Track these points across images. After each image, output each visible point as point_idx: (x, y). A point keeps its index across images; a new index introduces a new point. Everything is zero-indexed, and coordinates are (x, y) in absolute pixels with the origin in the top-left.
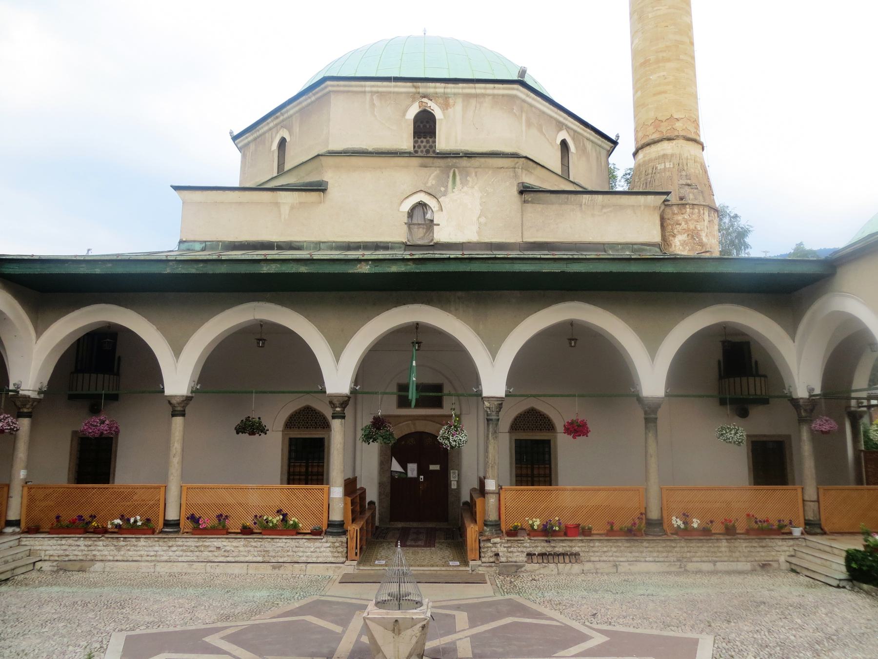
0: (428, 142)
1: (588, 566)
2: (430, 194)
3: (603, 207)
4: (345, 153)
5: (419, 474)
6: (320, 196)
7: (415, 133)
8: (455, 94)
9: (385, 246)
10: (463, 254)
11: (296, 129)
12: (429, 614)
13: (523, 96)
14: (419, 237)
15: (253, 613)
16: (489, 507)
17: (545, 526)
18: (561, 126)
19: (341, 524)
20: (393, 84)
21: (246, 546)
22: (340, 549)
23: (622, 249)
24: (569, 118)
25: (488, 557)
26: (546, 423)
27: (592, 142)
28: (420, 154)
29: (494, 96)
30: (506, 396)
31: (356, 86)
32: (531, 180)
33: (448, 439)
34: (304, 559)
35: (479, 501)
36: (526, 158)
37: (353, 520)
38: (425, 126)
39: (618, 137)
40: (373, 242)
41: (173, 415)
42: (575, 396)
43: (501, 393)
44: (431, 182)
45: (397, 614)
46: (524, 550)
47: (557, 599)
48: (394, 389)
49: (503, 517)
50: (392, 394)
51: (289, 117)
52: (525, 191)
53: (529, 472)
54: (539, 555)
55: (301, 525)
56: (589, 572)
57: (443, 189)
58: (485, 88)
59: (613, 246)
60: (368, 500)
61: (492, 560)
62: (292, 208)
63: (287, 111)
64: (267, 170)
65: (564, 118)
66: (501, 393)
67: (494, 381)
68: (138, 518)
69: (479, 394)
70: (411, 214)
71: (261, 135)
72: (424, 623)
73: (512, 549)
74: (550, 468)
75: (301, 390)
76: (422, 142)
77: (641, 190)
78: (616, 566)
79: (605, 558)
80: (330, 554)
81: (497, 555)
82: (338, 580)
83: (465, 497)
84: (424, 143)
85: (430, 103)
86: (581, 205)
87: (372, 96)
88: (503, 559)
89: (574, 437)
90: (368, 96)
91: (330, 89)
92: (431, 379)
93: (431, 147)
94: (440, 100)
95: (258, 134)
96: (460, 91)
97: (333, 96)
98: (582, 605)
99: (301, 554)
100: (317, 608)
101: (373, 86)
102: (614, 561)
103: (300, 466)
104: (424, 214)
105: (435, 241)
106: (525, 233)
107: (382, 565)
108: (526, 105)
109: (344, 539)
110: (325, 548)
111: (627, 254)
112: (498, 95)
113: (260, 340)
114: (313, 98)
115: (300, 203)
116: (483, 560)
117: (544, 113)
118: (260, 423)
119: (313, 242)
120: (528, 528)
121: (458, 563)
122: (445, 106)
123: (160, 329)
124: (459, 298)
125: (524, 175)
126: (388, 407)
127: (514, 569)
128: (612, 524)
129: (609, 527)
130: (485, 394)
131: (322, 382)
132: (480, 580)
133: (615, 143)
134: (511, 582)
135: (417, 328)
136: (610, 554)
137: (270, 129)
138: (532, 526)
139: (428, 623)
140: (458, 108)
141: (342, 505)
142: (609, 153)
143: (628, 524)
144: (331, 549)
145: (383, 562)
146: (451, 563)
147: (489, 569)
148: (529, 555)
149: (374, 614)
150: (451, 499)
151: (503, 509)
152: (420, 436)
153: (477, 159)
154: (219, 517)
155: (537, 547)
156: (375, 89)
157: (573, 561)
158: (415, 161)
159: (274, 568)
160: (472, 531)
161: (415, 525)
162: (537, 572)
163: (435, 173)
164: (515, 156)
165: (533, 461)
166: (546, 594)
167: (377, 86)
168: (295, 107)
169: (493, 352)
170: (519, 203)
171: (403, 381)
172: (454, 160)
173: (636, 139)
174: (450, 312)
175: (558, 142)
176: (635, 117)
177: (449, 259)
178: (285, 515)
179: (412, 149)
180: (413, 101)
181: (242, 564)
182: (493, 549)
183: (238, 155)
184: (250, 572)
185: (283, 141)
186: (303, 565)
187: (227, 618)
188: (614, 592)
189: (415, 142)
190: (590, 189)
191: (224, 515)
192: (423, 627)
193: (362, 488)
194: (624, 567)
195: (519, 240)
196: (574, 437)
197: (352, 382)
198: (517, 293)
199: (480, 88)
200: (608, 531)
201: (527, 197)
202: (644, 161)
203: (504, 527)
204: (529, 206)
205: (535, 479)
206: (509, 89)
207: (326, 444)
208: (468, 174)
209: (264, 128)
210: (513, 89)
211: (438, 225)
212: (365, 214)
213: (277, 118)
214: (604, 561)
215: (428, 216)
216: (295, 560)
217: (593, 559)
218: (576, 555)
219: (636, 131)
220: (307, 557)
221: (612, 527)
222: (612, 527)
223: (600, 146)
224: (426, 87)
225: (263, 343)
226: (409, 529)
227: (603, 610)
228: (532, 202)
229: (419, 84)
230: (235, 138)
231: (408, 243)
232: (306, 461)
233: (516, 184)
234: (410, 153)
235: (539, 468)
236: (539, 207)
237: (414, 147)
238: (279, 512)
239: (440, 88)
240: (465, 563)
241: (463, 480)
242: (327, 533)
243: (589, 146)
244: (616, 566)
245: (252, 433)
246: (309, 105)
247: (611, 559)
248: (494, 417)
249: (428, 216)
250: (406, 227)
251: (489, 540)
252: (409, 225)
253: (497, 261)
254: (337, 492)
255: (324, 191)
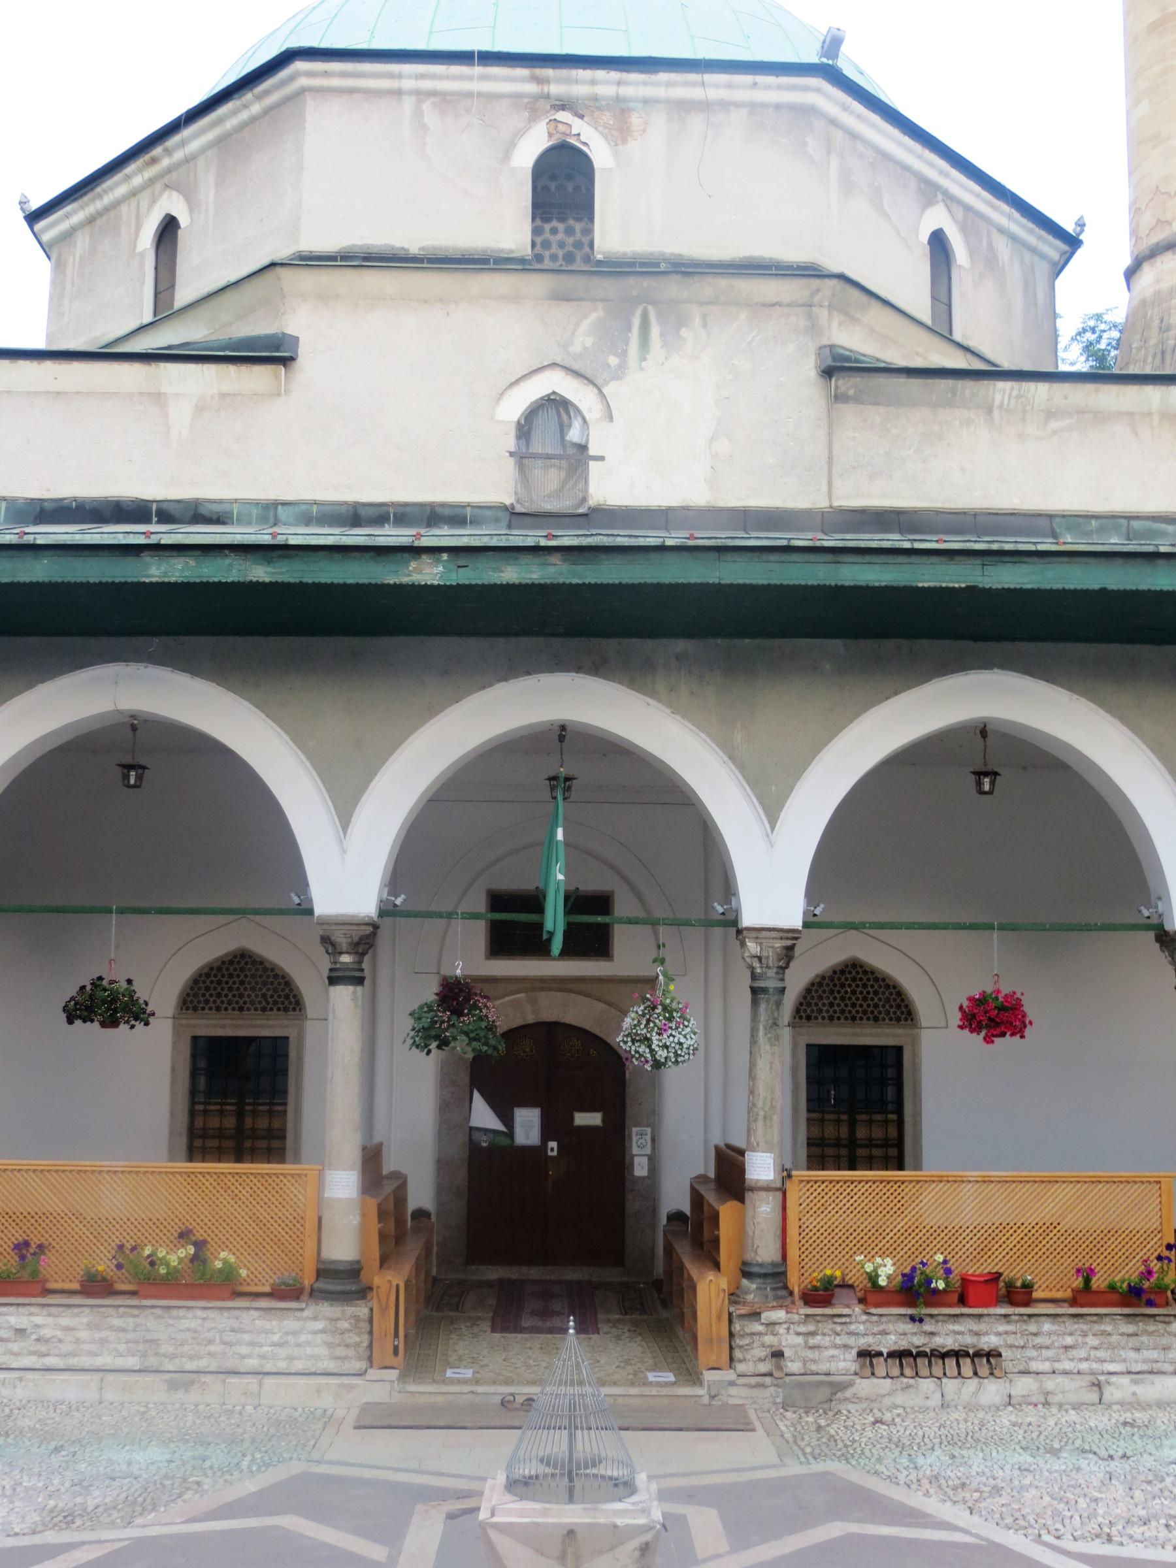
0: (570, 231)
1: (1023, 1386)
2: (577, 374)
3: (1050, 414)
4: (344, 258)
5: (546, 1136)
6: (277, 377)
7: (535, 205)
8: (646, 102)
9: (455, 516)
10: (692, 537)
11: (207, 191)
12: (657, 1515)
13: (832, 110)
14: (548, 492)
15: (135, 1506)
16: (756, 1227)
17: (908, 1278)
18: (930, 192)
19: (353, 1272)
20: (478, 70)
21: (98, 1327)
22: (353, 1338)
23: (1101, 530)
24: (954, 173)
25: (753, 1360)
26: (894, 1005)
27: (1013, 238)
28: (548, 263)
29: (753, 107)
30: (806, 925)
31: (375, 76)
32: (855, 339)
33: (647, 1040)
34: (252, 1363)
35: (727, 1211)
36: (842, 277)
37: (384, 1261)
38: (562, 187)
39: (1081, 225)
40: (422, 505)
41: (333, 981)
42: (990, 927)
43: (791, 916)
44: (583, 339)
45: (572, 1515)
46: (851, 1341)
47: (954, 1474)
48: (481, 906)
49: (793, 1253)
50: (476, 916)
51: (187, 160)
52: (838, 368)
53: (844, 1132)
54: (891, 1355)
55: (243, 1272)
56: (1026, 1401)
57: (613, 361)
58: (729, 86)
59: (1076, 520)
60: (412, 1205)
61: (763, 1368)
62: (200, 409)
63: (183, 144)
64: (123, 307)
65: (941, 172)
66: (791, 916)
67: (772, 883)
68: (223, 1255)
69: (731, 922)
70: (525, 428)
71: (107, 210)
72: (648, 1537)
73: (817, 1340)
74: (900, 1123)
75: (224, 905)
76: (554, 231)
77: (1148, 370)
78: (1098, 1385)
79: (1067, 1365)
80: (323, 1351)
81: (778, 1355)
82: (351, 1420)
83: (675, 1196)
84: (559, 232)
85: (578, 125)
86: (990, 410)
87: (419, 102)
88: (794, 1367)
89: (988, 1040)
90: (409, 103)
91: (303, 81)
92: (592, 884)
93: (578, 245)
94: (607, 118)
95: (99, 205)
96: (661, 92)
97: (310, 102)
98: (1023, 1488)
99: (244, 1350)
100: (312, 1494)
101: (422, 76)
102: (1092, 1373)
103: (221, 1113)
104: (563, 429)
105: (591, 502)
106: (838, 483)
107: (465, 1382)
108: (839, 135)
109: (361, 1310)
110: (310, 1336)
111: (1115, 542)
112: (765, 105)
113: (129, 767)
114: (256, 108)
115: (223, 395)
116: (741, 1367)
117: (885, 156)
118: (131, 994)
119: (256, 503)
120: (862, 1283)
121: (670, 1377)
122: (621, 133)
123: (299, 739)
124: (679, 657)
125: (835, 324)
126: (467, 956)
127: (832, 1390)
128: (1088, 1274)
129: (1079, 1282)
130: (748, 919)
131: (301, 883)
132: (736, 1422)
133: (1073, 242)
134: (819, 1428)
135: (561, 739)
136: (1082, 1353)
137: (134, 193)
138: (873, 1278)
139: (656, 1538)
140: (653, 135)
141: (355, 1220)
142: (1058, 269)
143: (1127, 1273)
144: (329, 1338)
145: (468, 1373)
146: (651, 1377)
147: (756, 1392)
148: (866, 1355)
149: (509, 1512)
150: (633, 1205)
151: (793, 1232)
152: (550, 1035)
153: (709, 279)
154: (21, 1247)
155: (885, 1333)
156: (426, 85)
157: (984, 1370)
158: (536, 284)
159: (173, 1386)
160: (710, 1289)
161: (534, 1273)
162: (887, 1401)
163: (593, 317)
164: (810, 272)
165: (858, 1104)
166: (921, 1461)
167: (434, 77)
168: (203, 131)
169: (771, 809)
170: (822, 403)
171: (514, 882)
172: (646, 282)
173: (1134, 233)
174: (653, 694)
175: (924, 237)
176: (1130, 173)
177: (662, 549)
178: (200, 1245)
179: (528, 251)
180: (533, 118)
181: (87, 1377)
182: (768, 1339)
183: (44, 267)
184: (109, 1396)
185: (169, 227)
186: (252, 1381)
187: (68, 1519)
188: (1103, 1453)
189: (536, 231)
190: (1006, 365)
191: (35, 1241)
192: (645, 1549)
193: (396, 1175)
194: (1120, 1389)
195: (822, 503)
196: (988, 1040)
197: (383, 885)
198: (837, 645)
199: (717, 86)
200: (1076, 1292)
201: (845, 384)
202: (1157, 293)
203: (795, 1281)
204: (848, 412)
205: (861, 1152)
206: (795, 88)
207: (292, 1054)
208: (682, 321)
209: (115, 189)
210: (807, 89)
211: (601, 458)
212: (395, 428)
213: (154, 161)
214: (1065, 1373)
215: (574, 434)
216: (230, 1364)
217: (1034, 1366)
218: (992, 1355)
219: (1136, 211)
220: (263, 1357)
221: (1087, 1281)
222: (1087, 1281)
223: (1034, 251)
224: (569, 81)
225: (139, 778)
226: (520, 1284)
227: (1082, 1503)
228: (857, 400)
229: (549, 72)
230: (33, 217)
231: (519, 509)
232: (239, 1096)
233: (812, 347)
234: (522, 261)
235: (870, 1122)
236: (876, 414)
237: (534, 244)
238: (184, 1235)
239: (605, 83)
240: (692, 1376)
241: (671, 1157)
242: (315, 1294)
243: (1003, 248)
244: (1098, 1385)
245: (111, 1022)
246: (243, 126)
247: (1084, 1366)
248: (771, 984)
249: (574, 434)
250: (511, 462)
251: (755, 1315)
252: (522, 458)
253: (795, 557)
254: (343, 1183)
255: (286, 361)
